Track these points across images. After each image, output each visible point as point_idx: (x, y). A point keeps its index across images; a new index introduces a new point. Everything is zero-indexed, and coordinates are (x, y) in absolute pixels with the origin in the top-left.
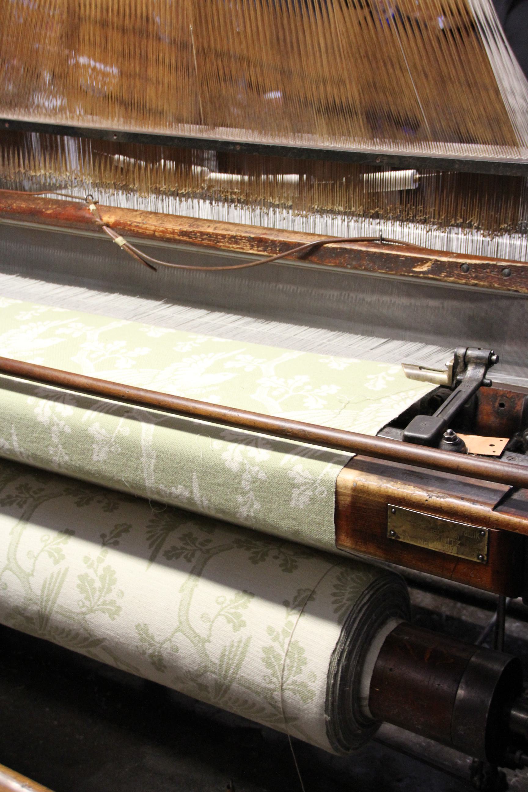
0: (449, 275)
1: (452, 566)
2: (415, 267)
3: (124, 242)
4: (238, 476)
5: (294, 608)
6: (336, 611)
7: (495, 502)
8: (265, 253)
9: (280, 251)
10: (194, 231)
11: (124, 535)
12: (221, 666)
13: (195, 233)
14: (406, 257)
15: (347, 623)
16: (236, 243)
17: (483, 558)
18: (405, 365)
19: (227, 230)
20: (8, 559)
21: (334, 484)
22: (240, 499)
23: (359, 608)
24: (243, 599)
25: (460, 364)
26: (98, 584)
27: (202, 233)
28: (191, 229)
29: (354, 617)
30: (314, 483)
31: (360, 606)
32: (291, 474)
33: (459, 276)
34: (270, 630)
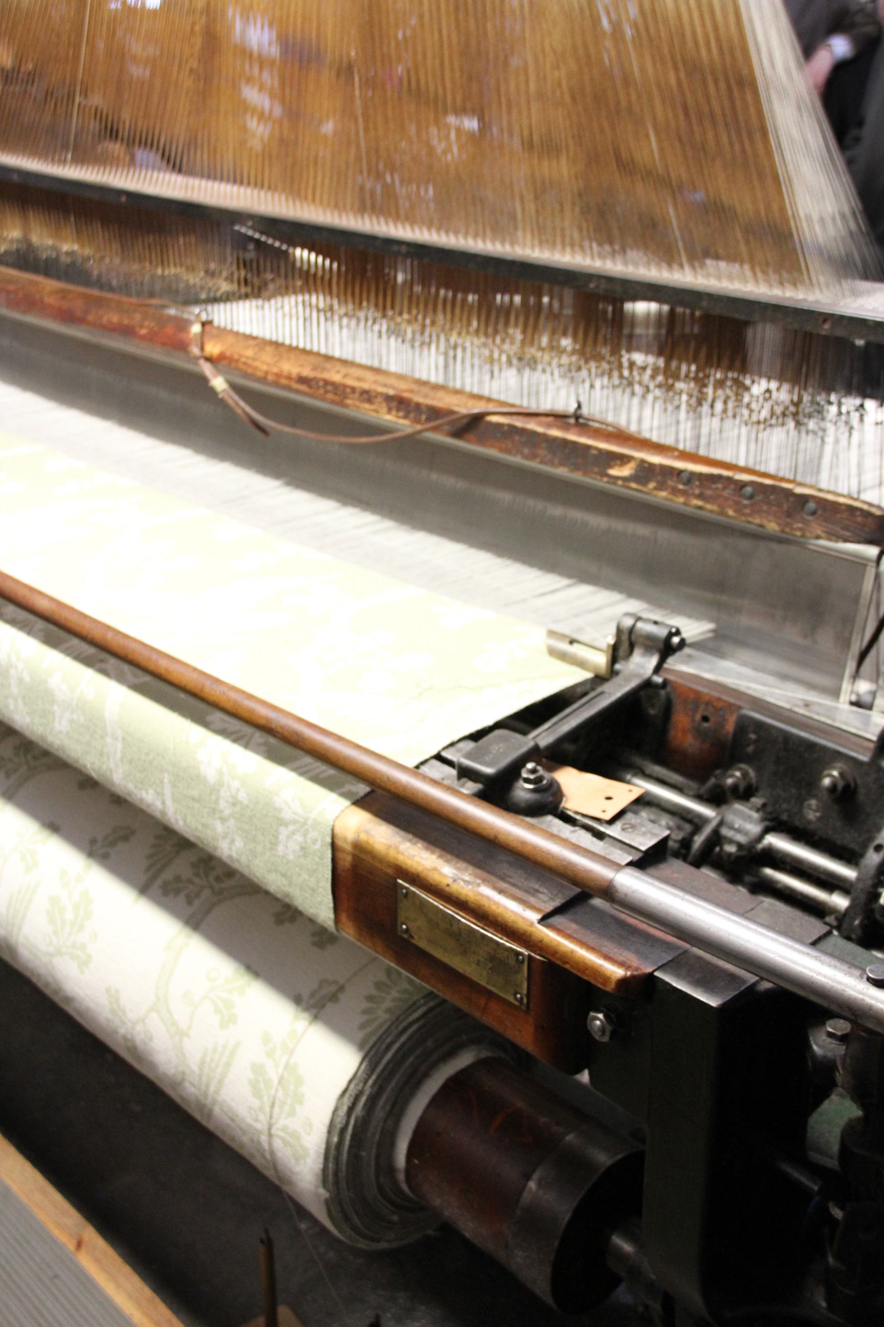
0: (661, 487)
1: (482, 1002)
2: (611, 467)
4: (215, 790)
5: (306, 1009)
6: (362, 1026)
7: (549, 907)
11: (121, 846)
12: (200, 1076)
13: (315, 379)
14: (599, 450)
15: (374, 1049)
17: (522, 998)
18: (552, 633)
21: (330, 832)
22: (219, 827)
23: (400, 1028)
25: (625, 643)
29: (388, 1040)
30: (305, 824)
31: (404, 1024)
32: (278, 802)
33: (675, 491)
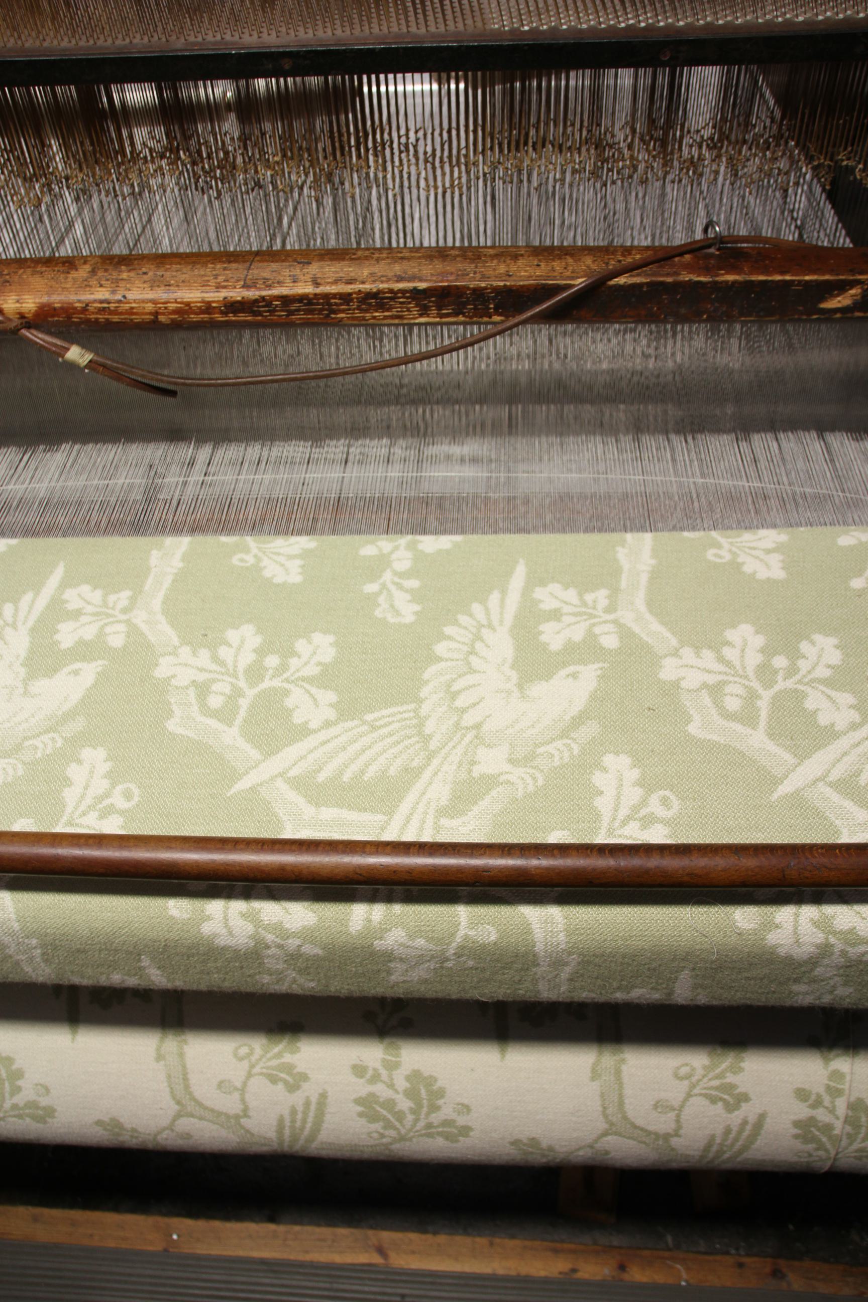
2: (823, 299)
3: (89, 357)
8: (461, 318)
10: (263, 298)
13: (267, 302)
16: (381, 306)
19: (350, 282)
20: (178, 1103)
24: (727, 1060)
26: (404, 1104)
27: (286, 300)
28: (252, 294)
34: (802, 1094)
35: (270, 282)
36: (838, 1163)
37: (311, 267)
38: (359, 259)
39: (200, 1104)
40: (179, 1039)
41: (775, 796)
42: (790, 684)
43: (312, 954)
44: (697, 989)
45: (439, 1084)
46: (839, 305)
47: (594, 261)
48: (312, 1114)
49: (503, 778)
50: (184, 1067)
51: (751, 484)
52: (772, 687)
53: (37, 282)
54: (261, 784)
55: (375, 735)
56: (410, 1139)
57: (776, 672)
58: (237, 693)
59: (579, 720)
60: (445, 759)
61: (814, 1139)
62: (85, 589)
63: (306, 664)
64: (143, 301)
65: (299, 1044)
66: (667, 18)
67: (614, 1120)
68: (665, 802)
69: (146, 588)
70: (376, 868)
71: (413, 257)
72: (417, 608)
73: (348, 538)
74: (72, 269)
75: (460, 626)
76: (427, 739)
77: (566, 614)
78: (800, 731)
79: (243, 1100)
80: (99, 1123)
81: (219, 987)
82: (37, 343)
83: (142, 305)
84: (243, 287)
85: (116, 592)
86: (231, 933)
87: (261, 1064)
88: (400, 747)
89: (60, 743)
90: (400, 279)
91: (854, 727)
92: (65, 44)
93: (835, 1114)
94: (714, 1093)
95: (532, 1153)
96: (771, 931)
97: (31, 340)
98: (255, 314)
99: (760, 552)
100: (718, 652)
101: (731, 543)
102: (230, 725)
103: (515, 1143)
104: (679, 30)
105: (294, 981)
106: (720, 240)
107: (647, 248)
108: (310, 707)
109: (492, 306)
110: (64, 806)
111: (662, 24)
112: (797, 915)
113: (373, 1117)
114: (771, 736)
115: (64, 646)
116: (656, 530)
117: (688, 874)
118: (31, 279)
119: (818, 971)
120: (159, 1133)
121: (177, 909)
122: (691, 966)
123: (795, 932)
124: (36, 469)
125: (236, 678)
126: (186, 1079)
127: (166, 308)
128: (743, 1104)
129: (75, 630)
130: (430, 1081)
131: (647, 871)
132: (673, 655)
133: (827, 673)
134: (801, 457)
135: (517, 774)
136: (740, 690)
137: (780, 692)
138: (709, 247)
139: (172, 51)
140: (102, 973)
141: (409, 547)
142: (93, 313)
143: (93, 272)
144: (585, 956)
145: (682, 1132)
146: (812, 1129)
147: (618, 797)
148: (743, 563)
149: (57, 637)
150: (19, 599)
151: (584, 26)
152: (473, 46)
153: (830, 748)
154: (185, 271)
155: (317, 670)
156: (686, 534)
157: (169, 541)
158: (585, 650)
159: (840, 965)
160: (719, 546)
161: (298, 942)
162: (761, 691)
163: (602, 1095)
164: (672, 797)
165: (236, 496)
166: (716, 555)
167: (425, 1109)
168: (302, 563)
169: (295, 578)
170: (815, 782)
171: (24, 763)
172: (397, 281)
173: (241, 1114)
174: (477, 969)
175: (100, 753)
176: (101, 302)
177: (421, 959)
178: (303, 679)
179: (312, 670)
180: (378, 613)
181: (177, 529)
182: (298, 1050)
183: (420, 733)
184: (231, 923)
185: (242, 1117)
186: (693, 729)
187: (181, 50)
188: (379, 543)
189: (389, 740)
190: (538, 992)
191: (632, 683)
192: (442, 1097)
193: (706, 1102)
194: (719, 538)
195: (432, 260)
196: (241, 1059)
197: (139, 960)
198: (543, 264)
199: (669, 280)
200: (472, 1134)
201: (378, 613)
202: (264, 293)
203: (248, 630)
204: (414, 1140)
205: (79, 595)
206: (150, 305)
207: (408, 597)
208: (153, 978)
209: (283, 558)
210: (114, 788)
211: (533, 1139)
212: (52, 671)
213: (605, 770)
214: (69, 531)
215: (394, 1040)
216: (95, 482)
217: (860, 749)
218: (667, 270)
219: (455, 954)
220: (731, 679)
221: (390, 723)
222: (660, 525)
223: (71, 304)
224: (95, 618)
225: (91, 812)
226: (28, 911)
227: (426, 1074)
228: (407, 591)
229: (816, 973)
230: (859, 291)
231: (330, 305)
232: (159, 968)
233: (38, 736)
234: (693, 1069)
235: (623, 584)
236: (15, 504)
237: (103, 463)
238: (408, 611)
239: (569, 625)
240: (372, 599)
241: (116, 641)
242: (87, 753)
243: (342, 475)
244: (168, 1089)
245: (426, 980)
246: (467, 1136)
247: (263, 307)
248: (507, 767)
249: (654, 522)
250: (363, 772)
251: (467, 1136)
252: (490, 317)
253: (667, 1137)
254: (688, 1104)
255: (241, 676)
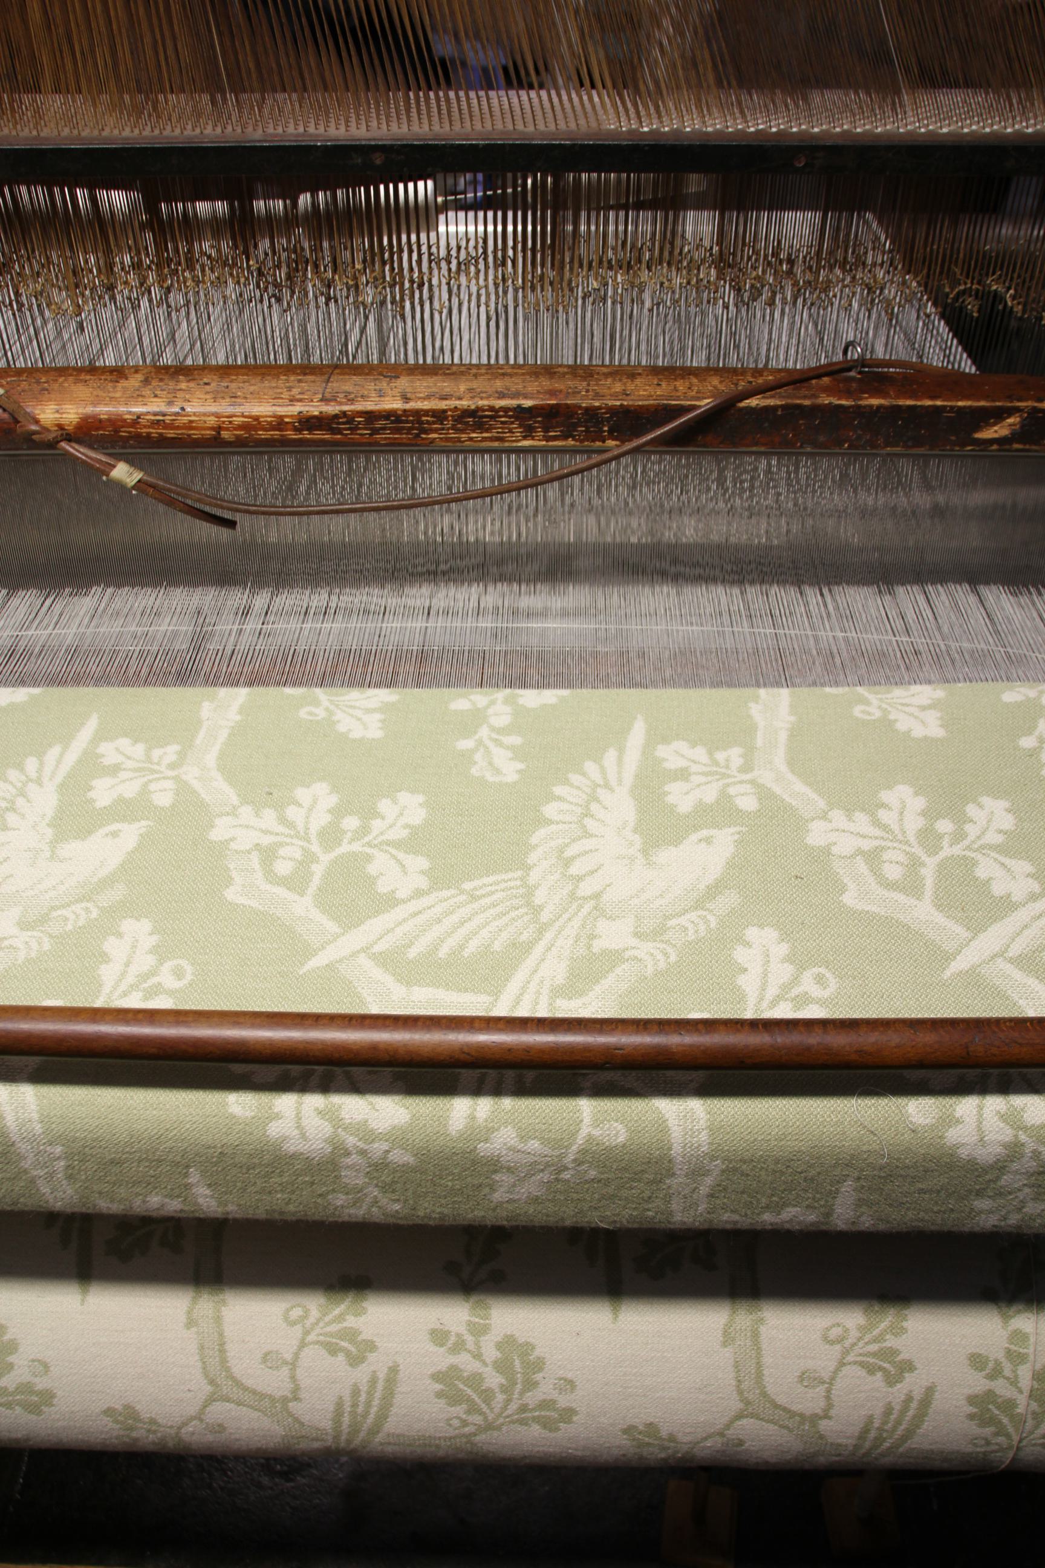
2: (978, 428)
3: (137, 476)
8: (570, 442)
9: (610, 432)
10: (344, 413)
16: (480, 426)
19: (443, 398)
20: (212, 1382)
24: (887, 1318)
26: (494, 1380)
27: (371, 416)
28: (331, 409)
34: (977, 1361)
35: (352, 396)
36: (1022, 1454)
37: (399, 381)
38: (453, 374)
39: (238, 1383)
40: (216, 1299)
41: (948, 973)
42: (957, 850)
43: (400, 1163)
44: (860, 1206)
45: (537, 1353)
46: (996, 436)
47: (721, 382)
48: (378, 1394)
49: (627, 954)
50: (221, 1335)
51: (898, 638)
52: (937, 853)
53: (82, 391)
54: (341, 960)
55: (476, 905)
56: (499, 1428)
57: (940, 837)
58: (310, 858)
59: (714, 890)
60: (560, 933)
61: (992, 1421)
62: (124, 743)
63: (391, 827)
64: (205, 414)
65: (365, 1304)
66: (800, 125)
67: (751, 1397)
68: (820, 980)
69: (198, 742)
70: (487, 1046)
71: (516, 374)
72: (520, 766)
73: (435, 691)
74: (121, 378)
75: (571, 785)
76: (537, 910)
77: (694, 773)
78: (970, 900)
79: (293, 1378)
80: (109, 1412)
81: (281, 1213)
82: (78, 458)
83: (203, 418)
84: (321, 400)
85: (162, 747)
86: (303, 1135)
87: (318, 1330)
88: (505, 919)
89: (95, 914)
90: (502, 396)
91: (1033, 897)
92: (127, 133)
93: (1017, 1389)
94: (871, 1360)
95: (649, 1444)
96: (950, 1127)
97: (72, 455)
98: (333, 431)
99: (916, 709)
100: (873, 814)
101: (881, 700)
102: (302, 894)
103: (628, 1430)
104: (814, 136)
105: (376, 1201)
106: (862, 362)
107: (780, 371)
108: (398, 874)
109: (606, 428)
110: (100, 985)
111: (794, 130)
112: (980, 1108)
113: (454, 1398)
114: (939, 907)
115: (99, 804)
116: (794, 685)
117: (856, 1052)
118: (73, 387)
119: (1005, 1180)
120: (185, 1424)
121: (239, 1105)
122: (856, 1174)
123: (979, 1128)
124: (61, 615)
125: (308, 842)
126: (222, 1351)
127: (230, 422)
128: (906, 1375)
129: (113, 786)
130: (526, 1349)
131: (808, 1048)
132: (821, 818)
133: (999, 839)
134: (954, 609)
135: (645, 949)
136: (901, 858)
137: (947, 858)
138: (849, 370)
139: (249, 142)
140: (138, 1194)
141: (506, 701)
142: (145, 427)
143: (146, 381)
144: (730, 1162)
145: (832, 1413)
146: (990, 1406)
147: (765, 974)
148: (896, 721)
149: (91, 795)
150: (45, 753)
151: (710, 129)
152: (588, 145)
153: (1007, 920)
154: (253, 382)
155: (405, 833)
156: (828, 690)
157: (223, 692)
158: (719, 812)
159: (1031, 1170)
160: (868, 703)
161: (385, 1146)
162: (924, 858)
163: (736, 1365)
164: (827, 975)
165: (300, 648)
166: (863, 712)
167: (519, 1386)
168: (383, 717)
169: (375, 733)
170: (993, 957)
171: (51, 936)
172: (499, 398)
173: (290, 1396)
174: (599, 1181)
175: (146, 925)
176: (155, 414)
177: (533, 1168)
178: (388, 843)
179: (399, 833)
180: (474, 771)
181: (232, 681)
182: (364, 1311)
183: (528, 904)
184: (305, 1122)
185: (290, 1401)
186: (849, 899)
187: (259, 141)
188: (472, 697)
189: (492, 911)
190: (671, 1213)
191: (775, 848)
192: (541, 1370)
193: (863, 1373)
194: (866, 694)
195: (537, 377)
196: (293, 1324)
197: (186, 1175)
198: (664, 384)
199: (807, 402)
200: (575, 1419)
201: (474, 771)
202: (345, 408)
203: (321, 788)
204: (504, 1428)
205: (117, 749)
206: (213, 418)
207: (510, 754)
208: (201, 1200)
209: (360, 712)
210: (162, 964)
211: (651, 1424)
212: (84, 833)
213: (748, 944)
214: (103, 680)
215: (482, 1297)
216: (133, 629)
217: (1040, 923)
218: (804, 392)
219: (575, 1160)
220: (890, 844)
221: (493, 893)
222: (798, 681)
223: (121, 415)
224: (137, 774)
225: (134, 993)
226: (55, 1109)
227: (521, 1340)
228: (507, 748)
229: (1002, 1182)
230: (1018, 419)
231: (421, 423)
232: (209, 1186)
233: (69, 906)
234: (847, 1330)
235: (759, 742)
236: (37, 650)
237: (141, 609)
238: (510, 770)
239: (699, 786)
240: (467, 757)
241: (163, 798)
242: (128, 925)
243: (424, 625)
244: (199, 1364)
245: (537, 1198)
246: (570, 1422)
247: (343, 423)
248: (633, 942)
249: (791, 677)
250: (462, 947)
251: (570, 1422)
252: (604, 442)
253: (814, 1419)
254: (841, 1374)
255: (314, 839)
